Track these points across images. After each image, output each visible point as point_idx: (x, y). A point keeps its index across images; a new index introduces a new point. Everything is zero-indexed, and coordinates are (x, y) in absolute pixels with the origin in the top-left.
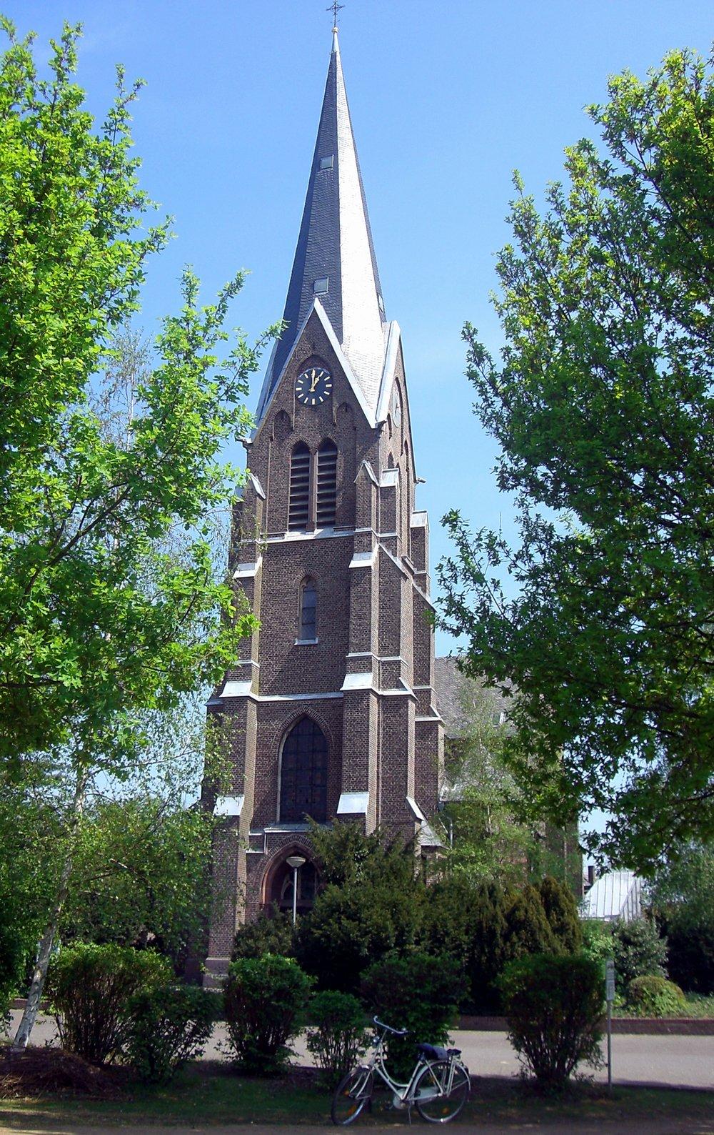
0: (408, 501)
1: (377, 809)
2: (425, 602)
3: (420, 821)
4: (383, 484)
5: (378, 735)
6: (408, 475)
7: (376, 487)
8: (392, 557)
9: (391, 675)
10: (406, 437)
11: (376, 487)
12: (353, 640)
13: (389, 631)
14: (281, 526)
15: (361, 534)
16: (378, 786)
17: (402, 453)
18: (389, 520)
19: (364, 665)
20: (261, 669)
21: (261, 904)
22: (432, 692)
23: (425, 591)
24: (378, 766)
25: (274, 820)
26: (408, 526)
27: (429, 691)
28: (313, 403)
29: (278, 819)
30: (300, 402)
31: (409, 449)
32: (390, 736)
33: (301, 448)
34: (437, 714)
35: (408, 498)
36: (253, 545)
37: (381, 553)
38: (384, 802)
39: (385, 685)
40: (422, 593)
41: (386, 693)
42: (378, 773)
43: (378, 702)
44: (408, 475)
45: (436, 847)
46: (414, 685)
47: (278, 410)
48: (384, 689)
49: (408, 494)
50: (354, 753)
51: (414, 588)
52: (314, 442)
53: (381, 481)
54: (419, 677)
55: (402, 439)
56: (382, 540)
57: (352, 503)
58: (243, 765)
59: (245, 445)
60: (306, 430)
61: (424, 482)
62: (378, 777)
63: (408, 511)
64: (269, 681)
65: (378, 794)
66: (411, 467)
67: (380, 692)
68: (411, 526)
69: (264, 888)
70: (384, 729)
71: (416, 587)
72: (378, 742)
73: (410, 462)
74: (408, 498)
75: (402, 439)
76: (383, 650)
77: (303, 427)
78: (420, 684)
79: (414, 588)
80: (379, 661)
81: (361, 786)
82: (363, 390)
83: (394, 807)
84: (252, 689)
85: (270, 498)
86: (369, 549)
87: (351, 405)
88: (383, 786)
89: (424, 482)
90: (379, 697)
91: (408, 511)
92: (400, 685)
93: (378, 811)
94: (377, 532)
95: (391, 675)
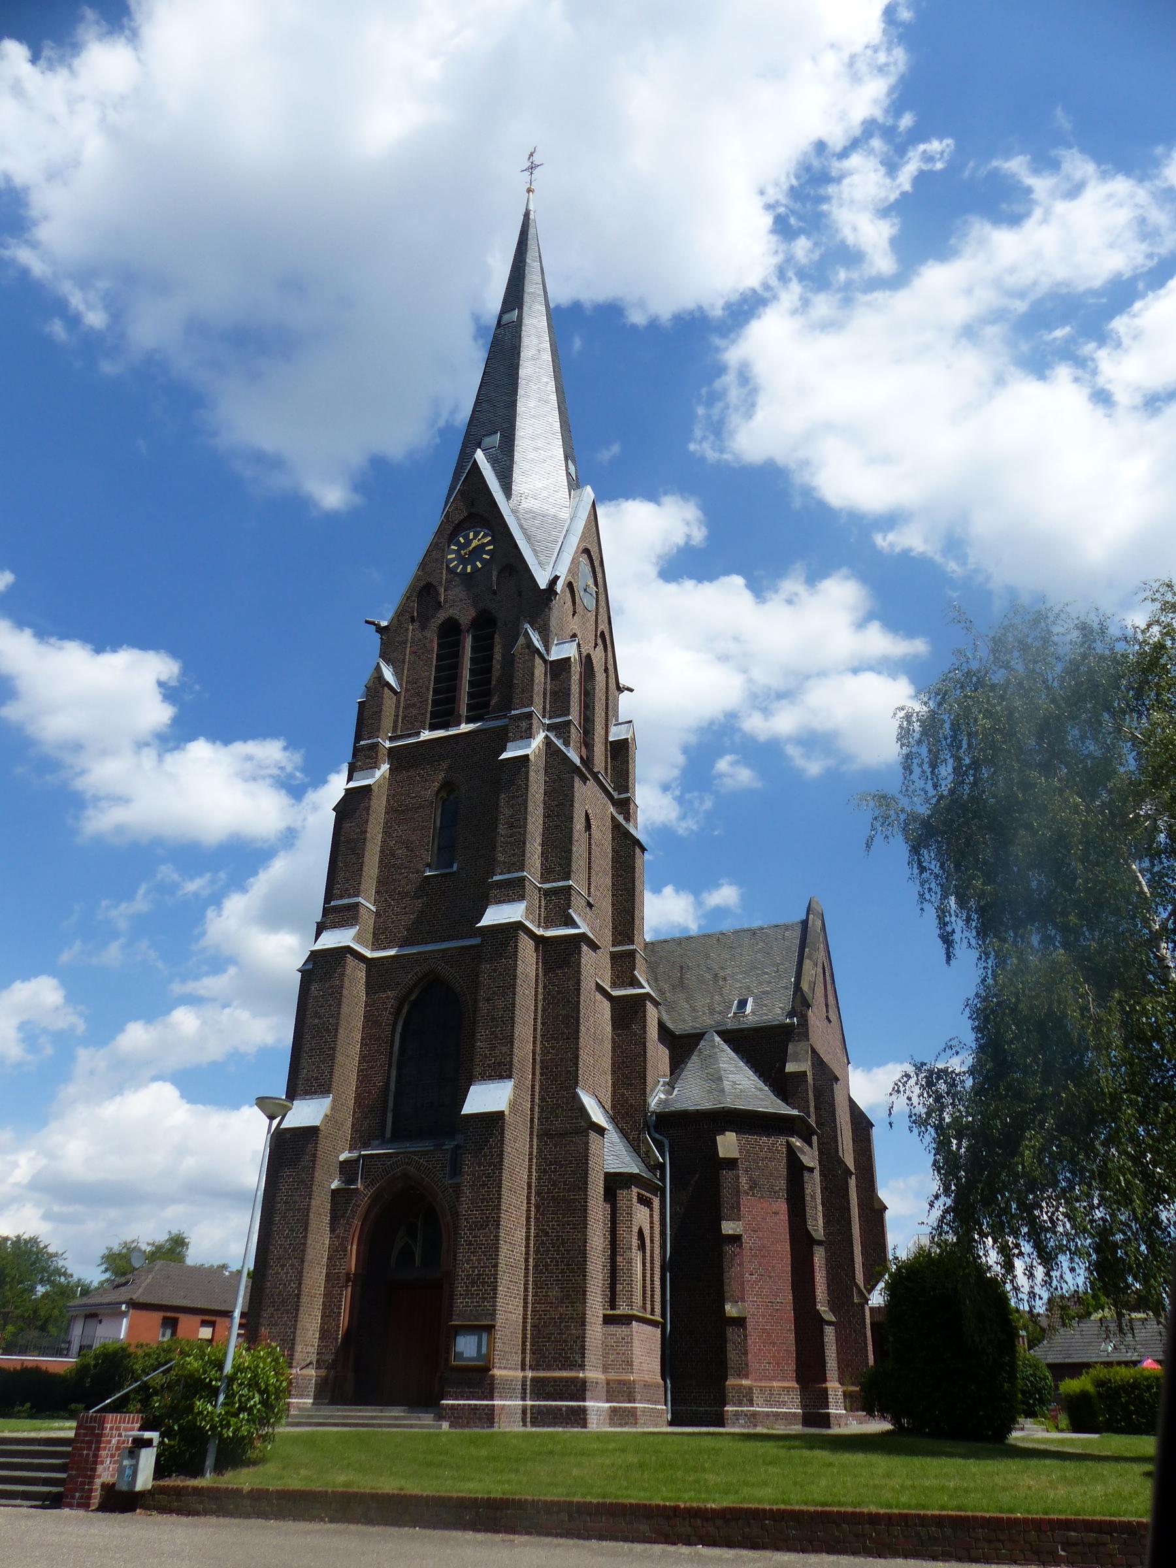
0: (607, 708)
1: (532, 1110)
2: (628, 834)
3: (601, 1131)
4: (555, 654)
5: (536, 995)
6: (607, 677)
7: (545, 661)
8: (563, 748)
9: (557, 906)
10: (603, 627)
11: (545, 661)
12: (501, 857)
13: (556, 847)
14: (417, 724)
15: (519, 717)
16: (534, 1074)
17: (596, 645)
18: (559, 701)
19: (513, 891)
20: (378, 914)
21: (348, 1274)
22: (638, 956)
23: (627, 819)
24: (534, 1043)
25: (383, 1135)
26: (607, 739)
27: (632, 954)
28: (469, 570)
29: (388, 1134)
30: (451, 571)
31: (609, 645)
32: (554, 997)
33: (450, 630)
34: (645, 984)
35: (607, 704)
36: (375, 746)
37: (548, 742)
38: (542, 1099)
39: (548, 923)
40: (623, 822)
41: (550, 933)
42: (534, 1053)
43: (536, 950)
44: (607, 677)
45: (631, 1175)
46: (613, 945)
47: (423, 583)
48: (546, 928)
49: (607, 699)
50: (493, 1019)
51: (613, 818)
52: (465, 614)
53: (554, 649)
54: (620, 934)
55: (597, 628)
56: (550, 728)
57: (508, 682)
58: (334, 1049)
59: (380, 630)
60: (459, 607)
61: (631, 690)
62: (534, 1059)
63: (607, 720)
64: (386, 929)
65: (533, 1086)
66: (611, 668)
67: (540, 932)
68: (611, 739)
69: (355, 1247)
70: (544, 987)
71: (616, 815)
72: (536, 1006)
73: (611, 661)
74: (607, 704)
75: (597, 628)
76: (546, 876)
77: (454, 601)
78: (621, 943)
79: (613, 818)
80: (540, 889)
81: (501, 1071)
82: (534, 551)
83: (558, 1106)
84: (358, 938)
85: (407, 690)
86: (529, 735)
87: (511, 563)
88: (542, 1074)
89: (631, 690)
90: (539, 940)
91: (607, 720)
92: (635, 983)
93: (532, 1114)
94: (544, 717)
95: (557, 906)
